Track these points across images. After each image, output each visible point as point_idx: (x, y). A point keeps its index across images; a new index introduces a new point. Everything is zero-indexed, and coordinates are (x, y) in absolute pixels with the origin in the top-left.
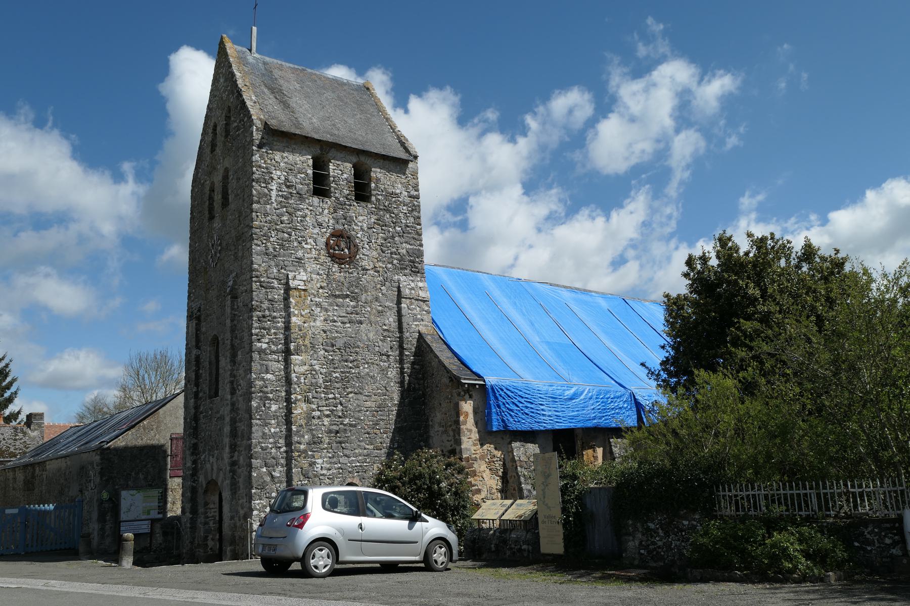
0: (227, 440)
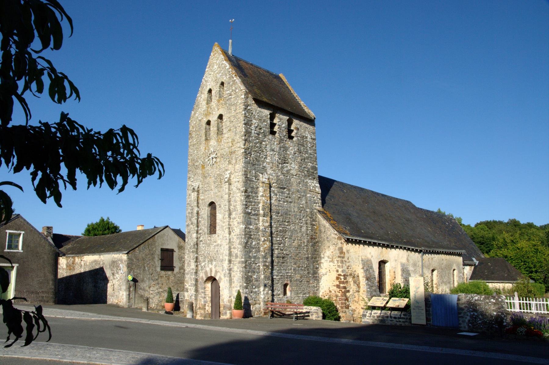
0: (227, 258)
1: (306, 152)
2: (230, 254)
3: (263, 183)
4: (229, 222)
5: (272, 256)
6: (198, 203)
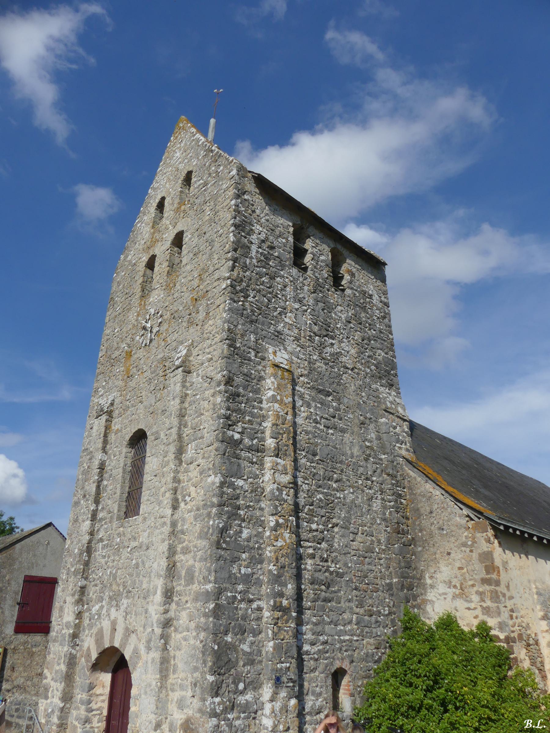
0: (159, 583)
1: (371, 326)
2: (171, 570)
3: (276, 366)
4: (176, 472)
5: (298, 577)
6: (105, 442)
